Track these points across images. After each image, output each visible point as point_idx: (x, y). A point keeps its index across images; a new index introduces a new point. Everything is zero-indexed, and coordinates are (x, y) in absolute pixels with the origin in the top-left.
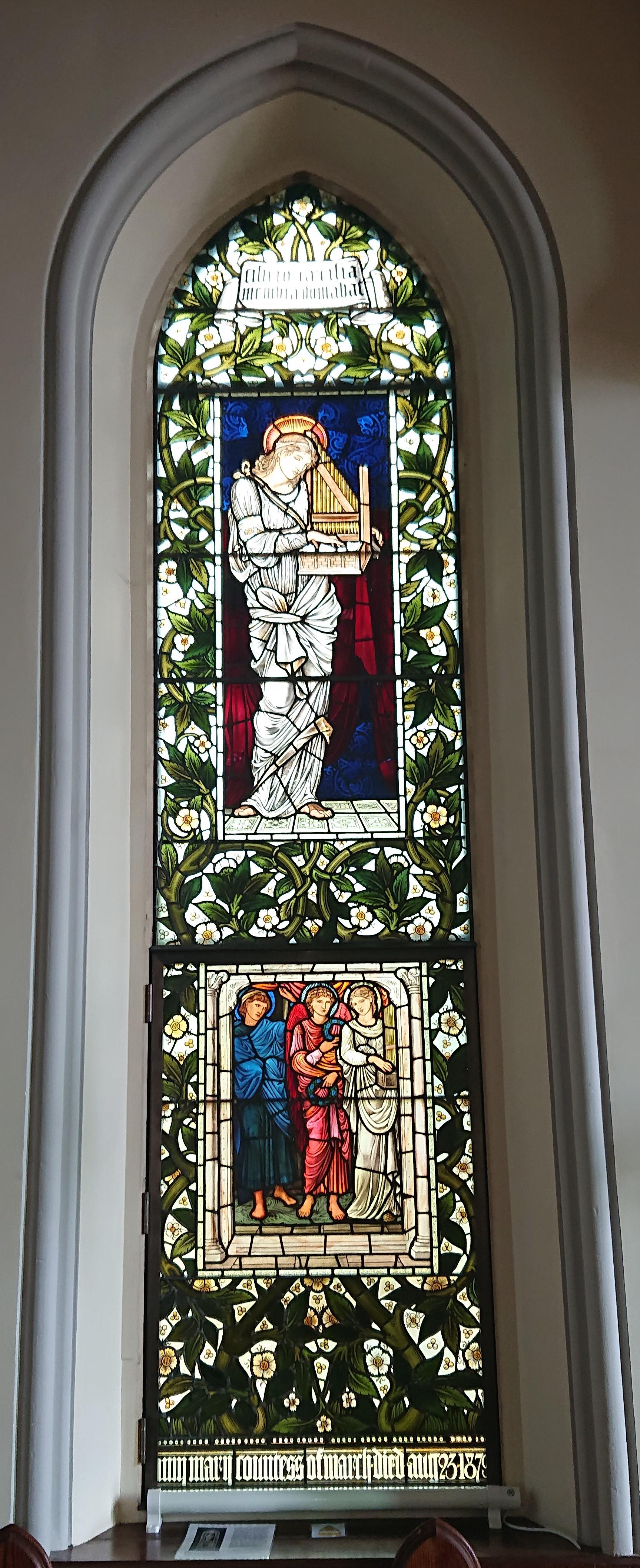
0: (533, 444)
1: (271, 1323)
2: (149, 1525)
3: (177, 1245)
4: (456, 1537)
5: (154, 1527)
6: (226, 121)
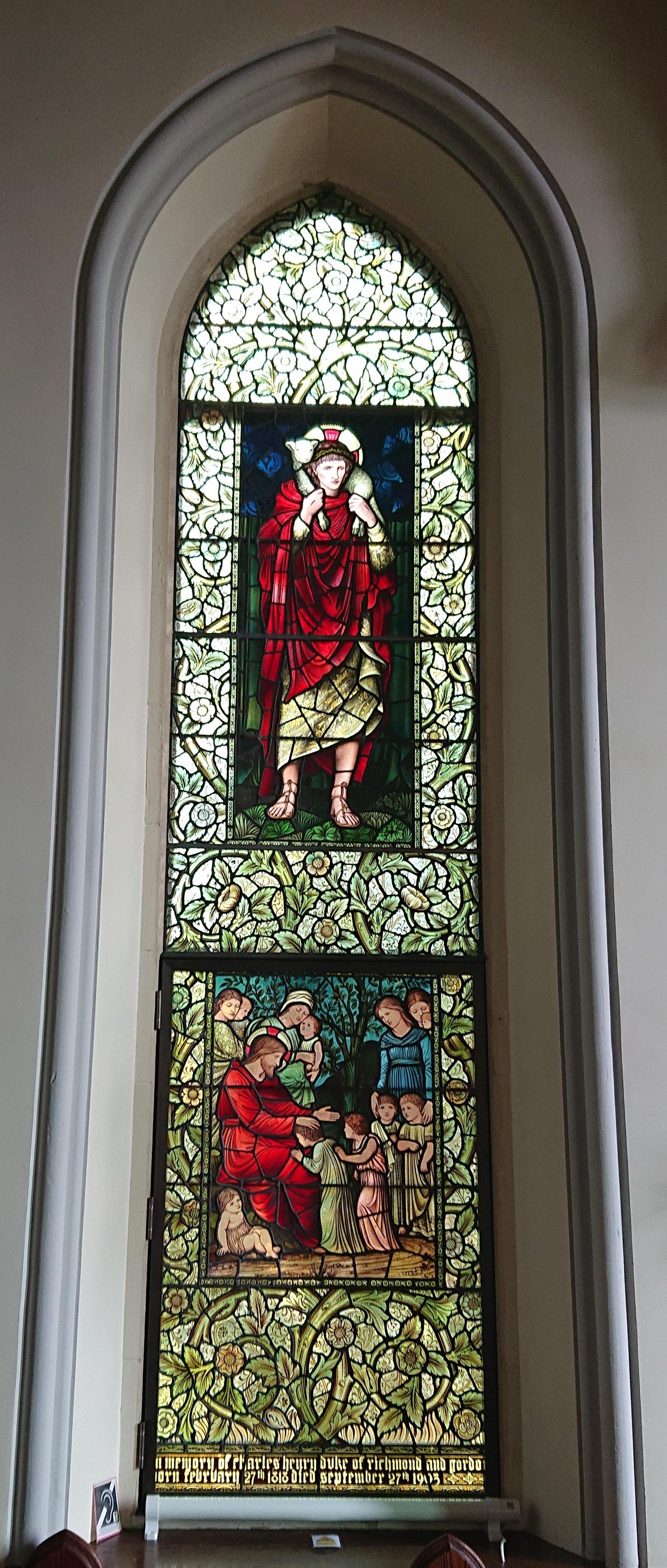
0: (560, 474)
1: (482, 1282)
2: (147, 1531)
3: (434, 879)
4: (463, 1549)
5: (153, 1533)
6: (245, 129)
